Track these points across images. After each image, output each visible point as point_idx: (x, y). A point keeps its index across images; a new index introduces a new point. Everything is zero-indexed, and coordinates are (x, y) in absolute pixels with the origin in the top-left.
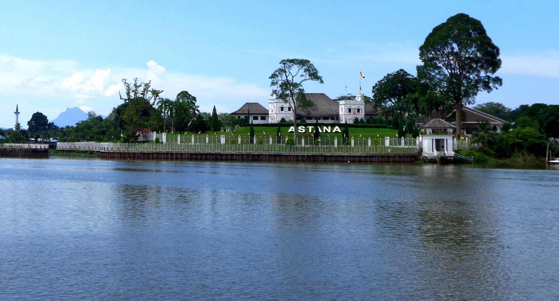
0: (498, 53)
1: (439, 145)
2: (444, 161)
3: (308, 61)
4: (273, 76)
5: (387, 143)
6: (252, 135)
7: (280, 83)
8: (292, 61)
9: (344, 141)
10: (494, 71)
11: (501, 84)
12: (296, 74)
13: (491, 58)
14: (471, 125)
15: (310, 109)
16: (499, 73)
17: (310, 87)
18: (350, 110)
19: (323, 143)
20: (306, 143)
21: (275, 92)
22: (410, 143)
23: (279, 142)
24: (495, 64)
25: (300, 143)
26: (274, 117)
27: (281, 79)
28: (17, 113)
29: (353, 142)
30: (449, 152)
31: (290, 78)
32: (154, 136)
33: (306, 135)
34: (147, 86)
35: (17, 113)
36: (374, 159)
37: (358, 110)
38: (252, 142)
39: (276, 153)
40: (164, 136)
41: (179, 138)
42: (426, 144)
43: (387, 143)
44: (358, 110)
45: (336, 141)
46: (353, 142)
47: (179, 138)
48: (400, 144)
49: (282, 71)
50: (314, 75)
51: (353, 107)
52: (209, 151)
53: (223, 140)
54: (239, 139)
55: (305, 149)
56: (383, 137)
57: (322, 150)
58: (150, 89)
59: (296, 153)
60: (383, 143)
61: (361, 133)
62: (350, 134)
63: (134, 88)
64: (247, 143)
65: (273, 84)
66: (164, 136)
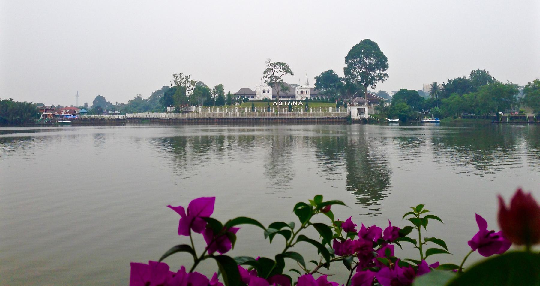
0: (387, 61)
1: (361, 111)
2: (364, 121)
3: (285, 63)
4: (265, 72)
5: (331, 110)
6: (253, 108)
7: (268, 77)
8: (277, 64)
9: (306, 109)
10: (384, 70)
11: (388, 77)
12: (279, 72)
13: (382, 62)
14: (376, 101)
15: (287, 91)
16: (387, 72)
17: (287, 79)
18: (302, 92)
19: (294, 111)
20: (285, 111)
21: (266, 82)
22: (344, 111)
23: (269, 111)
24: (385, 67)
25: (282, 111)
26: (259, 97)
27: (269, 75)
28: (77, 96)
29: (311, 110)
30: (366, 116)
31: (275, 74)
32: (193, 108)
33: (283, 106)
34: (187, 78)
35: (77, 96)
36: (334, 120)
37: (268, 92)
38: (254, 111)
39: (269, 117)
40: (200, 109)
41: (209, 109)
42: (354, 112)
43: (331, 110)
44: (307, 92)
45: (302, 110)
46: (311, 110)
47: (209, 109)
48: (338, 111)
49: (269, 69)
50: (289, 71)
51: (304, 90)
52: (230, 117)
53: (236, 110)
54: (246, 109)
55: (313, 115)
56: (328, 107)
57: (296, 115)
58: (190, 80)
59: (280, 117)
60: (328, 111)
61: (316, 105)
62: (309, 106)
63: (179, 80)
64: (251, 111)
65: (265, 77)
66: (200, 109)
